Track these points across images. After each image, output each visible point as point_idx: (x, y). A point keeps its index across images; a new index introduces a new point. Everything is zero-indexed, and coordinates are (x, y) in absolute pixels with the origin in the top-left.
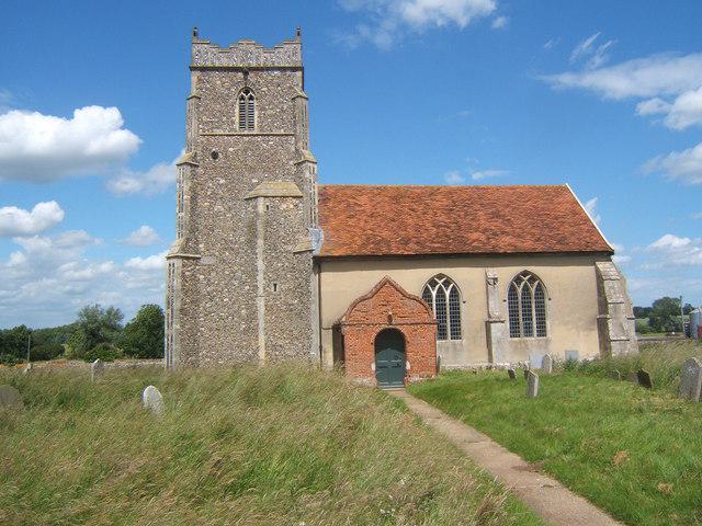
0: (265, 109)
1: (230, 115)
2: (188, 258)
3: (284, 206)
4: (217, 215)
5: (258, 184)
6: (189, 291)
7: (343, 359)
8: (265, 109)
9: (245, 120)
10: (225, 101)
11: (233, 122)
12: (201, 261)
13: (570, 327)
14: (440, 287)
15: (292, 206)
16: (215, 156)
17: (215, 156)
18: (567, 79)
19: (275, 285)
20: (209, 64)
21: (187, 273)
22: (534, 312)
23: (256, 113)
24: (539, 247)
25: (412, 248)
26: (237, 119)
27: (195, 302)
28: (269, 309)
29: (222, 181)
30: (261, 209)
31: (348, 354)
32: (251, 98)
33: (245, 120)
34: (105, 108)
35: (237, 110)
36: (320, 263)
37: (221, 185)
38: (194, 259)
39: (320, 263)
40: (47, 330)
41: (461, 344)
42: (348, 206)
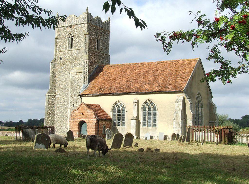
5: (72, 68)
9: (70, 46)
11: (66, 46)
15: (79, 76)
16: (61, 59)
17: (61, 59)
19: (73, 105)
21: (50, 101)
26: (67, 45)
27: (53, 111)
29: (62, 68)
30: (70, 78)
32: (72, 37)
33: (70, 46)
35: (68, 42)
36: (81, 96)
37: (62, 69)
38: (53, 95)
40: (166, 153)
41: (124, 128)
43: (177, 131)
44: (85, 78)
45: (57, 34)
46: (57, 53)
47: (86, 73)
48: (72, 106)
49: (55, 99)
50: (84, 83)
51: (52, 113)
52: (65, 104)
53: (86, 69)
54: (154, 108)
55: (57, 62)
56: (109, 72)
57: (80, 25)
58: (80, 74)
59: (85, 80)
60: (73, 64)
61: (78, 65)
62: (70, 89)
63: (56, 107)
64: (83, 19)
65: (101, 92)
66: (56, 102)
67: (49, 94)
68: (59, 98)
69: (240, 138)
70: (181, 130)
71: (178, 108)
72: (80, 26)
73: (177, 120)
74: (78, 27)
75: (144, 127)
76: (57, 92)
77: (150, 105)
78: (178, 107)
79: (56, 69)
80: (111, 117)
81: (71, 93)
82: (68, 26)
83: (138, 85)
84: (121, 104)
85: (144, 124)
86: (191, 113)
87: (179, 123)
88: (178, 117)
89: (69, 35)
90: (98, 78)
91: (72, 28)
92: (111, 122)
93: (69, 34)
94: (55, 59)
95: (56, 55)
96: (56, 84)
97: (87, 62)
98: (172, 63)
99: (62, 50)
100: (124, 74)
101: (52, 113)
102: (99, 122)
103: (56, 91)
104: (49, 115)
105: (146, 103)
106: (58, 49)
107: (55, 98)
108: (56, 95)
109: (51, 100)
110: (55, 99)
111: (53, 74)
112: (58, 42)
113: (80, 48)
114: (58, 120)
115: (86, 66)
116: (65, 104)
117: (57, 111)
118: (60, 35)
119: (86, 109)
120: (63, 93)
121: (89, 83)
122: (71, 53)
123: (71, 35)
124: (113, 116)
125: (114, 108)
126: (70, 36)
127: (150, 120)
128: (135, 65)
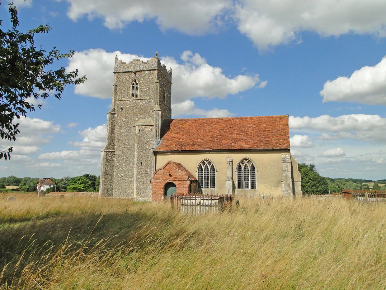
0: (142, 89)
1: (128, 92)
2: (109, 152)
3: (146, 130)
4: (122, 134)
5: (138, 120)
6: (109, 164)
7: (294, 194)
8: (142, 89)
9: (134, 93)
10: (127, 86)
11: (129, 95)
12: (115, 153)
13: (267, 184)
14: (246, 165)
15: (149, 130)
16: (122, 109)
17: (122, 109)
18: (10, 88)
19: (141, 163)
20: (129, 71)
22: (250, 177)
23: (138, 90)
24: (255, 147)
25: (196, 148)
26: (131, 93)
27: (112, 169)
28: (138, 173)
29: (124, 120)
30: (137, 131)
31: (296, 193)
33: (134, 93)
34: (380, 62)
36: (155, 153)
37: (123, 121)
38: (112, 152)
39: (155, 153)
42: (179, 128)
43: (287, 194)
44: (158, 132)
45: (117, 80)
46: (117, 102)
47: (158, 126)
48: (140, 164)
49: (114, 156)
50: (157, 138)
51: (110, 173)
52: (128, 162)
53: (158, 122)
54: (253, 168)
55: (116, 113)
56: (182, 127)
57: (148, 72)
58: (150, 127)
59: (157, 134)
60: (139, 116)
61: (145, 117)
62: (136, 145)
63: (116, 165)
64: (152, 65)
65: (183, 149)
66: (115, 159)
67: (108, 150)
68: (119, 156)
69: (211, 209)
70: (292, 193)
71: (286, 168)
72: (147, 72)
73: (286, 181)
74: (146, 73)
75: (240, 189)
76: (116, 148)
77: (248, 164)
78: (287, 167)
79: (115, 121)
80: (197, 178)
81: (138, 149)
82: (131, 72)
83: (229, 142)
84: (210, 163)
85: (240, 186)
86: (299, 174)
87: (289, 185)
88: (287, 178)
89: (133, 82)
90: (171, 133)
91: (137, 74)
92: (197, 184)
93: (132, 81)
94: (114, 109)
95: (115, 105)
96: (116, 139)
97: (159, 113)
98: (258, 119)
99: (124, 99)
100: (203, 129)
101: (110, 173)
102: (192, 184)
103: (115, 146)
104: (107, 174)
105: (242, 162)
106: (117, 97)
107: (114, 155)
108: (115, 152)
109: (109, 157)
110: (114, 156)
111: (112, 127)
112: (117, 90)
113: (149, 97)
114: (118, 181)
115: (158, 119)
116: (128, 162)
117: (117, 171)
118: (120, 81)
119: (175, 168)
120: (125, 150)
121: (161, 138)
122: (136, 103)
123: (135, 81)
124: (199, 176)
125: (200, 167)
126: (134, 83)
127: (247, 181)
128: (213, 120)
